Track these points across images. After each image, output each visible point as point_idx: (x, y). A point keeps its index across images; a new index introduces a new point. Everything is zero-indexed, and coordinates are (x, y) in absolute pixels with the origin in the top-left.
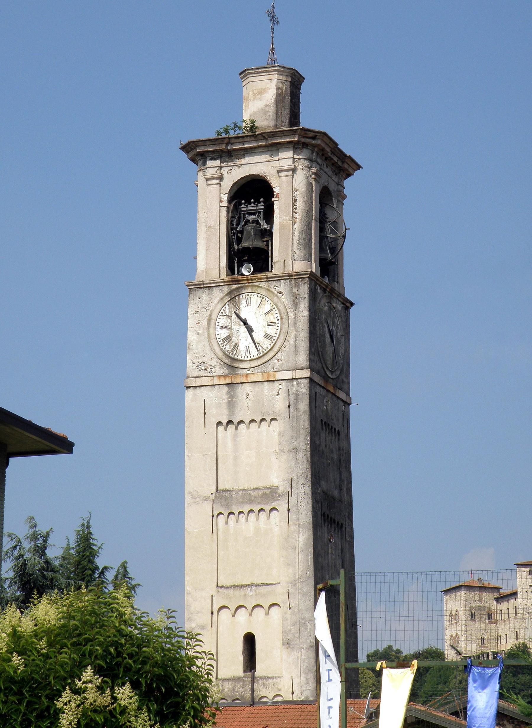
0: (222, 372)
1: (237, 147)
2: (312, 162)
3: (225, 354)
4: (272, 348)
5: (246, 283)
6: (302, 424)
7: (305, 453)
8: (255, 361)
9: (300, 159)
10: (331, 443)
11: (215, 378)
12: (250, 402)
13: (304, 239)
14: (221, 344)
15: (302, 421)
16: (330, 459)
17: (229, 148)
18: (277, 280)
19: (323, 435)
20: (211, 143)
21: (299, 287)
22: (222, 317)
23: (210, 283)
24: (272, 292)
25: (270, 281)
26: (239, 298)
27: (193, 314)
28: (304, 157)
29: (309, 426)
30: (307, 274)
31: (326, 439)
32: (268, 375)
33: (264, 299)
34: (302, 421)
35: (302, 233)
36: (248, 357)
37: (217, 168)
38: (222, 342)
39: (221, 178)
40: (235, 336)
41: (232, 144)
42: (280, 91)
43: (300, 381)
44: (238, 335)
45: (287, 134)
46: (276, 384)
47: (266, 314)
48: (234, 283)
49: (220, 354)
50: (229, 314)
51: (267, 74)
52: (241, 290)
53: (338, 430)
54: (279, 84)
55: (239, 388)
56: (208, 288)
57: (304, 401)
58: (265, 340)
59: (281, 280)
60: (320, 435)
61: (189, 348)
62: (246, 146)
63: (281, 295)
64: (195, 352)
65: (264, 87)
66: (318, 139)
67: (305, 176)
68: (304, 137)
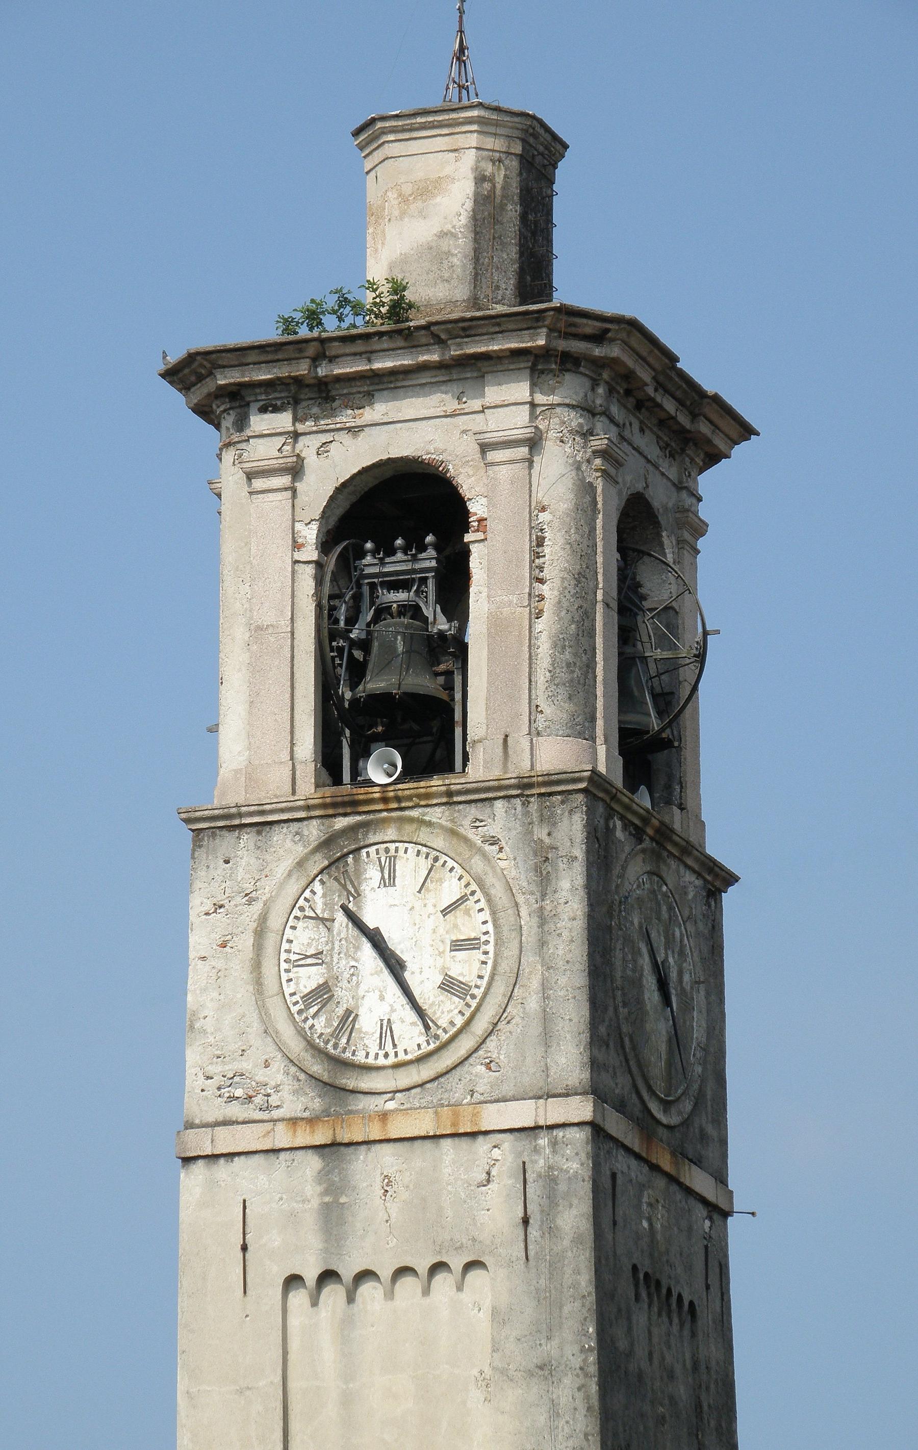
0: (300, 1107)
1: (348, 370)
2: (594, 415)
3: (311, 1045)
4: (468, 1023)
5: (380, 811)
7: (580, 1381)
8: (413, 1069)
9: (552, 406)
10: (669, 1347)
11: (280, 1127)
12: (394, 1209)
13: (568, 665)
14: (300, 1012)
15: (568, 1271)
16: (666, 1401)
17: (321, 372)
19: (641, 1319)
21: (554, 824)
22: (300, 925)
23: (262, 813)
24: (466, 840)
25: (460, 803)
26: (357, 860)
27: (207, 914)
28: (567, 401)
30: (579, 780)
31: (650, 1332)
33: (441, 862)
34: (568, 1271)
35: (564, 647)
36: (386, 1056)
37: (282, 439)
39: (296, 470)
40: (344, 984)
41: (332, 359)
42: (487, 186)
43: (561, 1134)
45: (511, 326)
47: (445, 912)
48: (341, 811)
49: (296, 1046)
50: (323, 911)
51: (445, 131)
52: (366, 835)
53: (691, 1304)
54: (483, 164)
56: (255, 829)
57: (575, 1201)
58: (443, 996)
59: (495, 799)
60: (629, 1319)
61: (192, 1027)
63: (495, 848)
64: (211, 1039)
66: (612, 340)
67: (571, 461)
68: (568, 336)
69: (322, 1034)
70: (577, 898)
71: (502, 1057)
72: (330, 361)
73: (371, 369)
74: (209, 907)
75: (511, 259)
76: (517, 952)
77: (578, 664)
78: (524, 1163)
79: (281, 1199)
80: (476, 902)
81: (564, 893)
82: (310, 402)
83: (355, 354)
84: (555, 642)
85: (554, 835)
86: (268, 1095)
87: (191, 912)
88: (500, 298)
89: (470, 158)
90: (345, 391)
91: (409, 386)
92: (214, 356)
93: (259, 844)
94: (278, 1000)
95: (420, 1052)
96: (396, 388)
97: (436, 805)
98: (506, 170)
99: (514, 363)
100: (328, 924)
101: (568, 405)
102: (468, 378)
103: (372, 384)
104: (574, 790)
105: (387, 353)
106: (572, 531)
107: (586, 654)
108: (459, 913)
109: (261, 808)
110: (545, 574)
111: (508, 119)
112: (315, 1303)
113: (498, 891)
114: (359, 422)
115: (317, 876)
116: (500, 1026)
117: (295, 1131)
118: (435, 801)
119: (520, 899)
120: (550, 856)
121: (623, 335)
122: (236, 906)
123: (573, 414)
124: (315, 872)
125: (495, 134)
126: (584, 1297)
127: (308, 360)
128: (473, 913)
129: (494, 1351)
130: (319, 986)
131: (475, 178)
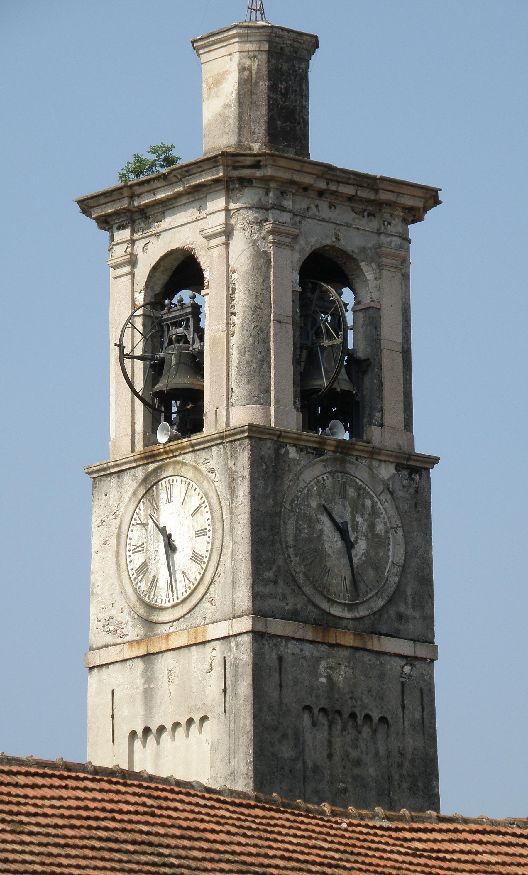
0: (135, 634)
1: (147, 201)
2: (267, 210)
4: (202, 578)
5: (166, 459)
6: (242, 724)
7: (246, 781)
8: (180, 607)
9: (238, 210)
11: (126, 646)
12: (172, 688)
13: (248, 362)
14: (135, 579)
15: (242, 718)
17: (136, 204)
18: (207, 448)
20: (107, 200)
21: (236, 458)
22: (135, 528)
23: (118, 465)
24: (200, 471)
25: (198, 450)
26: (157, 488)
27: (99, 526)
28: (245, 205)
29: (251, 728)
30: (243, 432)
32: (196, 632)
33: (191, 486)
34: (242, 718)
35: (245, 352)
36: (169, 601)
37: (126, 245)
38: (135, 576)
39: (132, 262)
40: (152, 561)
41: (139, 196)
42: (246, 73)
44: (156, 560)
45: (206, 167)
46: (208, 647)
47: (193, 515)
48: (150, 461)
49: (133, 598)
51: (224, 44)
52: (161, 473)
54: (244, 61)
55: (158, 662)
56: (116, 475)
57: (245, 677)
59: (213, 446)
61: (92, 592)
62: (158, 197)
63: (213, 475)
64: (100, 599)
65: (221, 72)
66: (266, 166)
67: (248, 241)
68: (235, 168)
69: (144, 591)
70: (246, 500)
71: (216, 597)
72: (138, 197)
73: (156, 200)
74: (99, 522)
75: (263, 115)
76: (221, 535)
77: (254, 361)
78: (225, 657)
79: (128, 688)
80: (205, 507)
81: (241, 498)
82: (140, 221)
83: (148, 192)
84: (240, 350)
85: (236, 464)
86: (123, 629)
87: (92, 525)
88: (255, 139)
89: (236, 57)
90: (153, 213)
91: (179, 206)
92: (86, 202)
93: (119, 483)
94: (126, 573)
95: (183, 597)
96: (173, 207)
97: (188, 452)
98: (259, 61)
99: (217, 187)
100: (146, 527)
101: (246, 208)
102: (202, 198)
103: (163, 207)
104: (243, 437)
105: (161, 189)
106: (250, 282)
107: (260, 354)
108: (198, 515)
109: (116, 463)
110: (236, 311)
111: (256, 31)
112: (144, 746)
113: (214, 501)
114: (158, 230)
115: (141, 500)
116: (216, 578)
117: (132, 649)
118: (187, 451)
119: (223, 504)
120: (235, 477)
121: (271, 162)
122: (110, 520)
123: (250, 212)
124: (140, 497)
125: (248, 41)
126: (248, 732)
127: (127, 198)
128: (204, 513)
129: (211, 767)
130: (143, 563)
131: (239, 70)
